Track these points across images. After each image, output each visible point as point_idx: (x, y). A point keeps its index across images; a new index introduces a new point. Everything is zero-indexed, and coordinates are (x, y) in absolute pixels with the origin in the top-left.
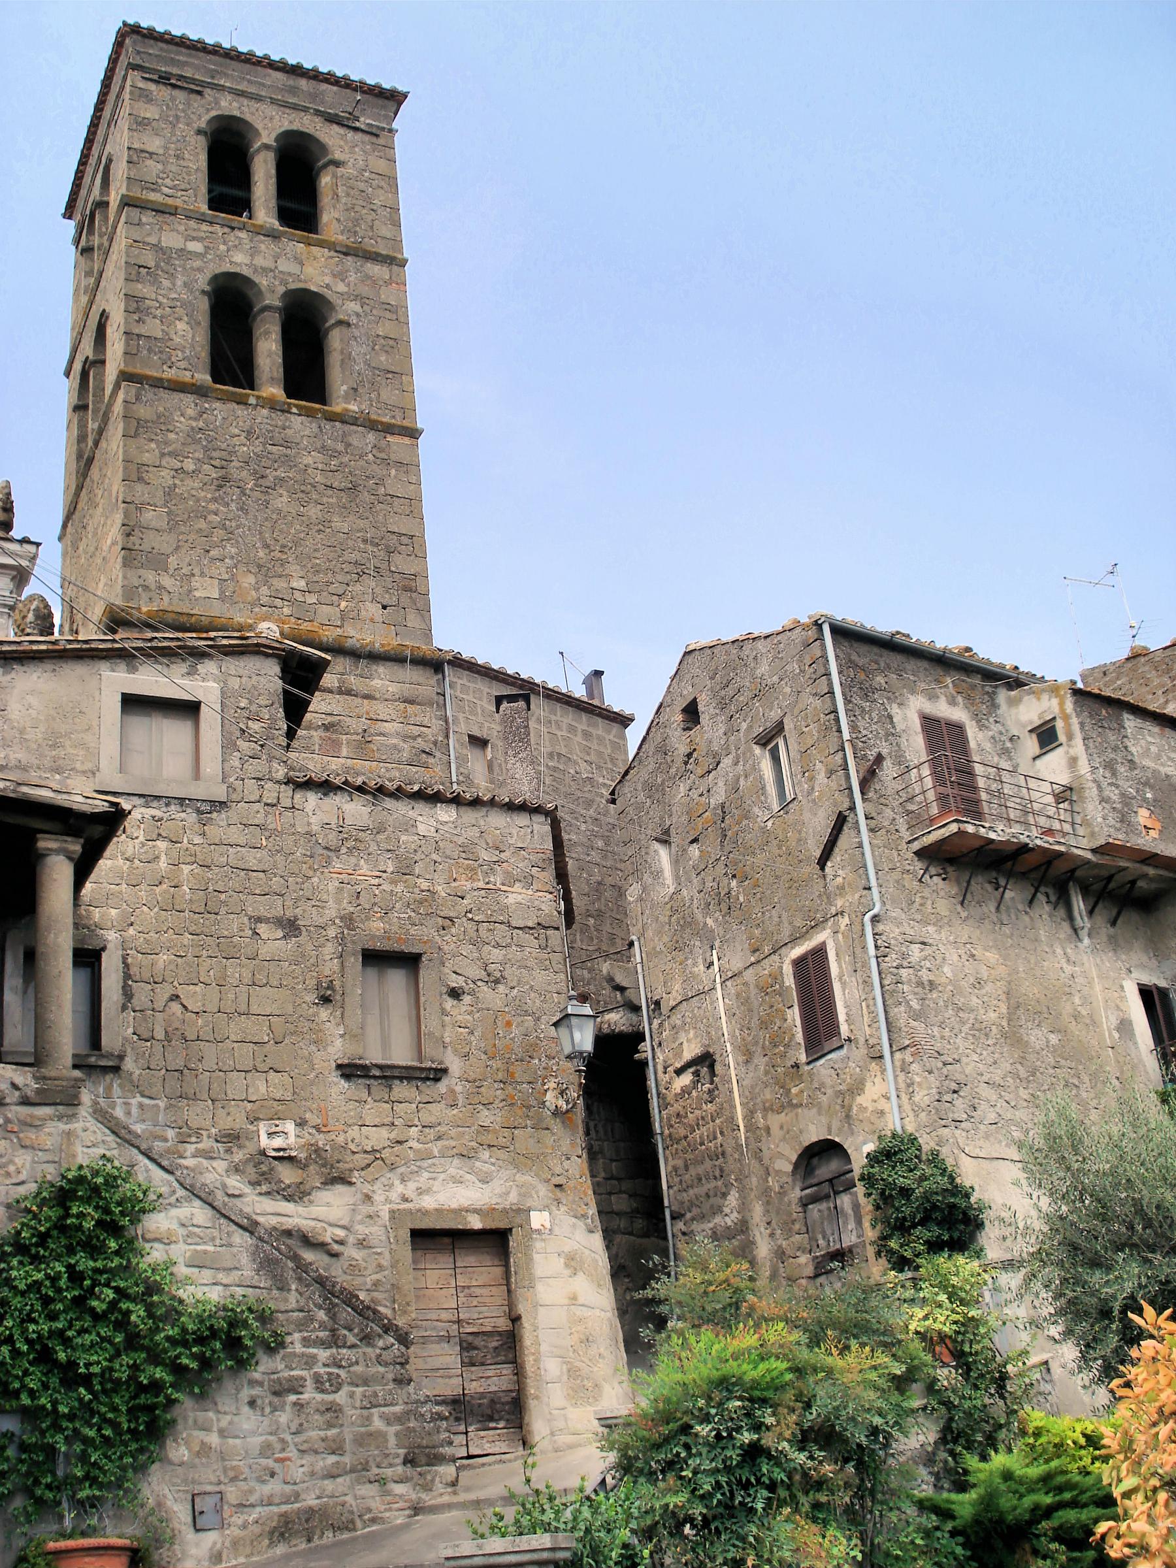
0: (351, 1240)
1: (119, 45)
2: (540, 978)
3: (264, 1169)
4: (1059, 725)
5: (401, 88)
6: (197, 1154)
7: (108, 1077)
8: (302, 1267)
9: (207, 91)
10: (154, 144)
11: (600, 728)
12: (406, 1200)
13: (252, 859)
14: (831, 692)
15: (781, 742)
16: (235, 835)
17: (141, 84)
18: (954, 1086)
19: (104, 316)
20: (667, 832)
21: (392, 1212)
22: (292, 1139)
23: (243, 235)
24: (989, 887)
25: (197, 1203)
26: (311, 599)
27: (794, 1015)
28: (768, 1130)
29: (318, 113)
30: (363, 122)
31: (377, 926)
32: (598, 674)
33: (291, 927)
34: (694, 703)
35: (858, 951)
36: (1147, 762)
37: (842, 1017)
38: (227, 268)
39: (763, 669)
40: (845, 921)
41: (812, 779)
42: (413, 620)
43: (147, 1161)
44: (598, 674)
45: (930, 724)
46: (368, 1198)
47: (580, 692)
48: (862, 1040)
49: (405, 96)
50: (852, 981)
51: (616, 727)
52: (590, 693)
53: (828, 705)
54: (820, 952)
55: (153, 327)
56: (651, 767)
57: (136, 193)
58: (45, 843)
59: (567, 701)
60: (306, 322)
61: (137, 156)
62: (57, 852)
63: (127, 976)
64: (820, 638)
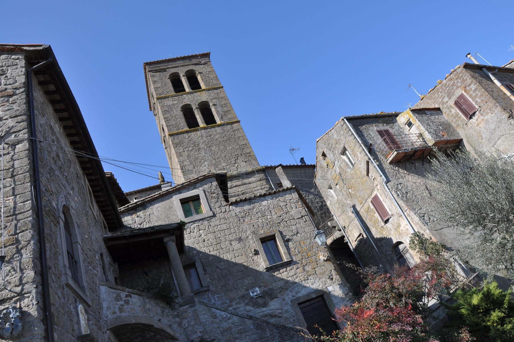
0: (283, 311)
1: (145, 68)
2: (307, 229)
3: (254, 302)
4: (411, 120)
5: (208, 52)
6: (236, 304)
7: (207, 293)
8: (268, 323)
9: (167, 70)
10: (159, 85)
11: (307, 170)
12: (294, 296)
13: (224, 227)
14: (353, 134)
15: (347, 152)
16: (218, 222)
17: (152, 74)
18: (422, 215)
19: (162, 125)
20: (330, 185)
21: (291, 301)
22: (259, 292)
23: (185, 95)
24: (411, 165)
25: (234, 316)
26: (228, 167)
27: (377, 215)
28: (382, 245)
29: (192, 64)
30: (203, 62)
31: (262, 232)
32: (302, 159)
33: (240, 240)
34: (323, 153)
35: (385, 192)
36: (436, 120)
37: (388, 210)
38: (184, 104)
39: (335, 136)
40: (379, 187)
41: (357, 156)
42: (253, 162)
43: (218, 311)
44: (302, 159)
45: (381, 133)
46: (284, 299)
47: (299, 164)
48: (395, 214)
49: (210, 53)
50: (387, 200)
51: (311, 169)
52: (302, 163)
53: (353, 137)
54: (376, 197)
55: (172, 122)
56: (321, 172)
57: (159, 96)
58: (166, 240)
59: (297, 167)
60: (205, 109)
61: (156, 89)
62: (169, 241)
63: (203, 266)
64: (345, 123)
